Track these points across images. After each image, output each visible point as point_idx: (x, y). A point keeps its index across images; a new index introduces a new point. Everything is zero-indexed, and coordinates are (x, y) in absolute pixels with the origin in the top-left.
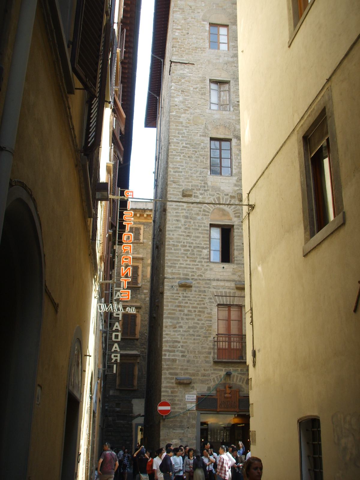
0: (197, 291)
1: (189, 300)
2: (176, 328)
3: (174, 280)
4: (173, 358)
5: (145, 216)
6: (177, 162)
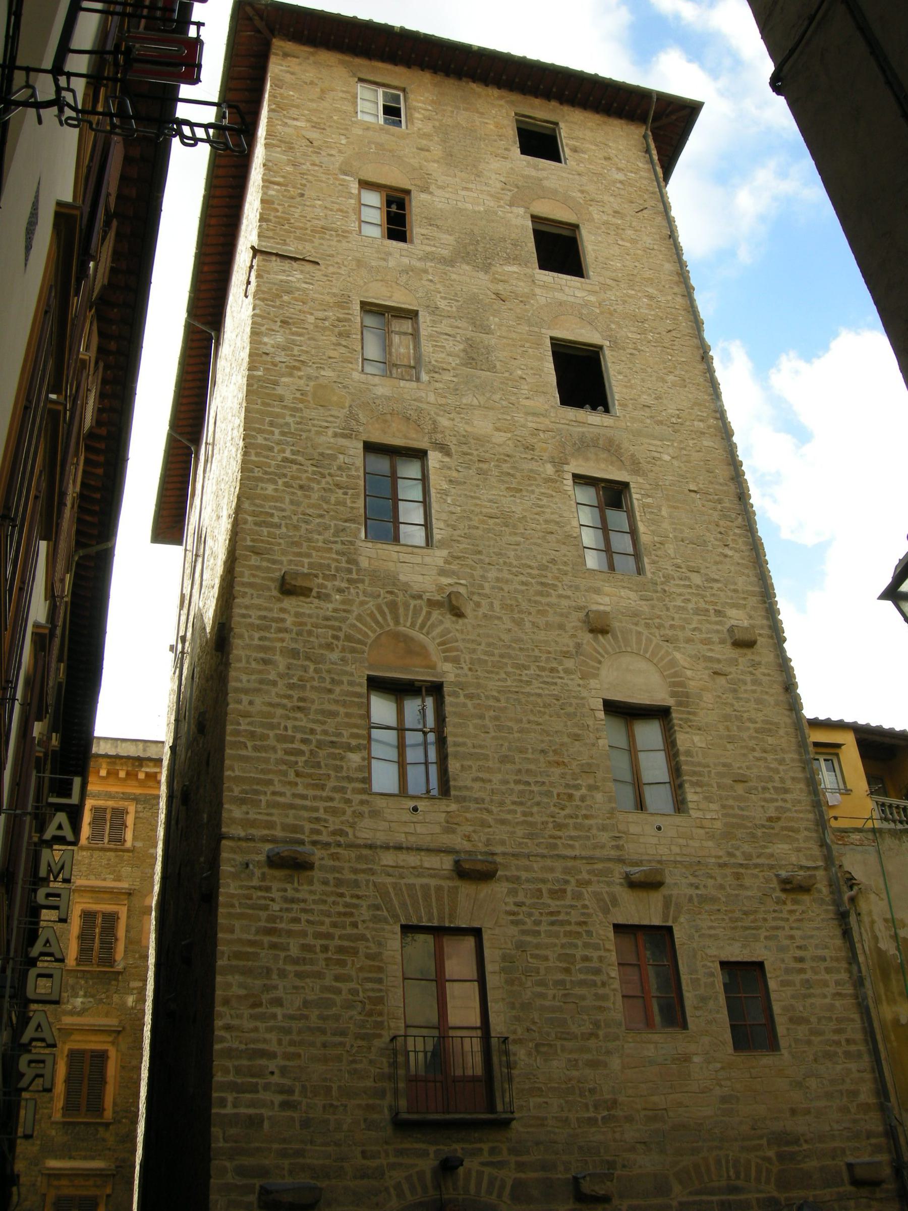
0: (332, 882)
1: (304, 911)
2: (259, 1004)
3: (251, 844)
4: (251, 1111)
5: (141, 776)
6: (266, 498)
